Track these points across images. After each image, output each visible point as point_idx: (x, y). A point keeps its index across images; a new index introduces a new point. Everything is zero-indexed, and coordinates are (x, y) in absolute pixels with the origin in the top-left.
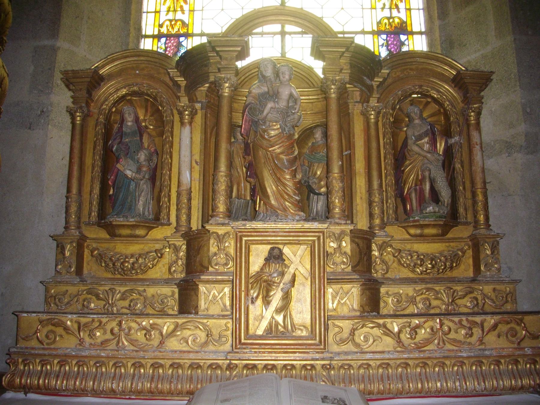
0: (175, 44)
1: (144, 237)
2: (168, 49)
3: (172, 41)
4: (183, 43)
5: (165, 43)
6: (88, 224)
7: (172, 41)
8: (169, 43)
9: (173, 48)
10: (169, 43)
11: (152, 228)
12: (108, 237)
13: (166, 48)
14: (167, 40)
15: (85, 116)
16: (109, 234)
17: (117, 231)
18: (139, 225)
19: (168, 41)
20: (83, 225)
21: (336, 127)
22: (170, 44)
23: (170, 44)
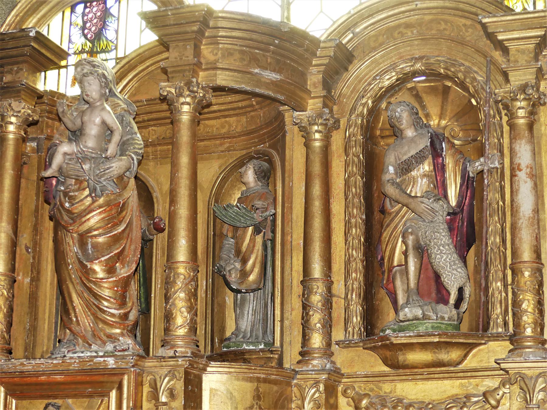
0: (99, 14)
1: (460, 363)
2: (88, 25)
3: (95, 9)
4: (112, 11)
5: (84, 14)
6: (345, 344)
7: (95, 9)
8: (89, 13)
9: (95, 21)
10: (89, 13)
11: (471, 347)
12: (386, 369)
13: (85, 23)
14: (86, 7)
15: (534, 105)
16: (386, 362)
17: (401, 358)
18: (412, 344)
19: (87, 10)
20: (335, 348)
21: (187, 182)
22: (90, 16)
23: (90, 16)
